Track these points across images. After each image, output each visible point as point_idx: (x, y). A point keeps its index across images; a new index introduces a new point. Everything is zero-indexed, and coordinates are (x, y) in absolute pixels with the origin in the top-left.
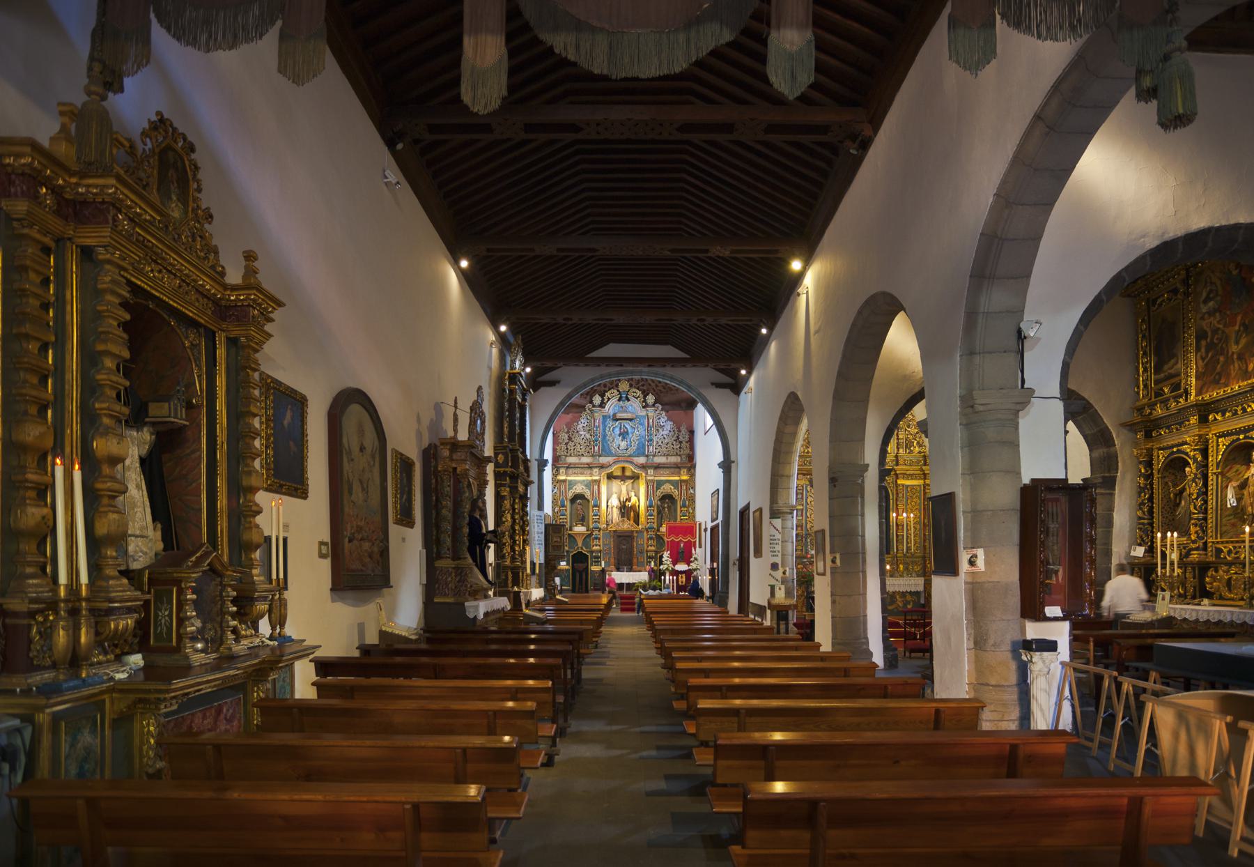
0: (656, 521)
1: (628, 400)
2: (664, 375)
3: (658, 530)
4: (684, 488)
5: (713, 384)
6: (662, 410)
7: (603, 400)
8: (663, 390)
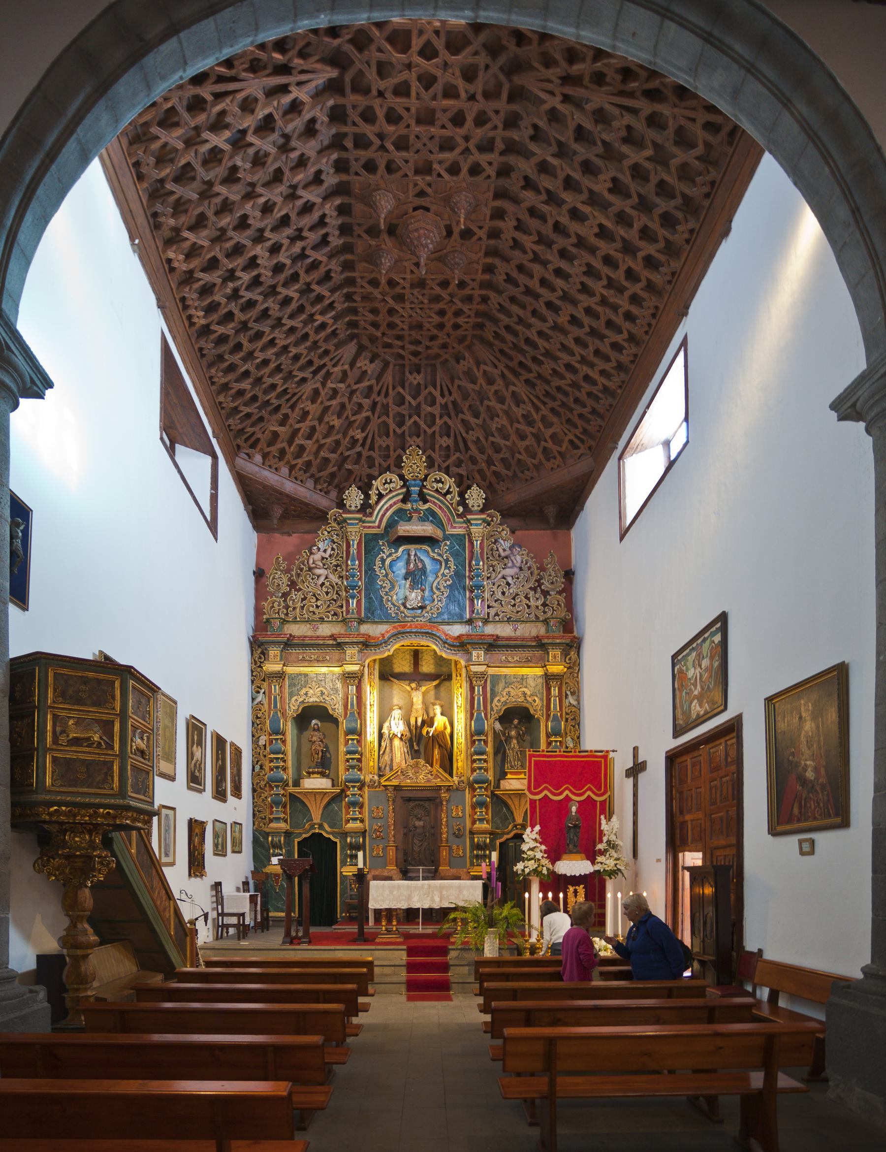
3: (498, 786)
7: (367, 496)
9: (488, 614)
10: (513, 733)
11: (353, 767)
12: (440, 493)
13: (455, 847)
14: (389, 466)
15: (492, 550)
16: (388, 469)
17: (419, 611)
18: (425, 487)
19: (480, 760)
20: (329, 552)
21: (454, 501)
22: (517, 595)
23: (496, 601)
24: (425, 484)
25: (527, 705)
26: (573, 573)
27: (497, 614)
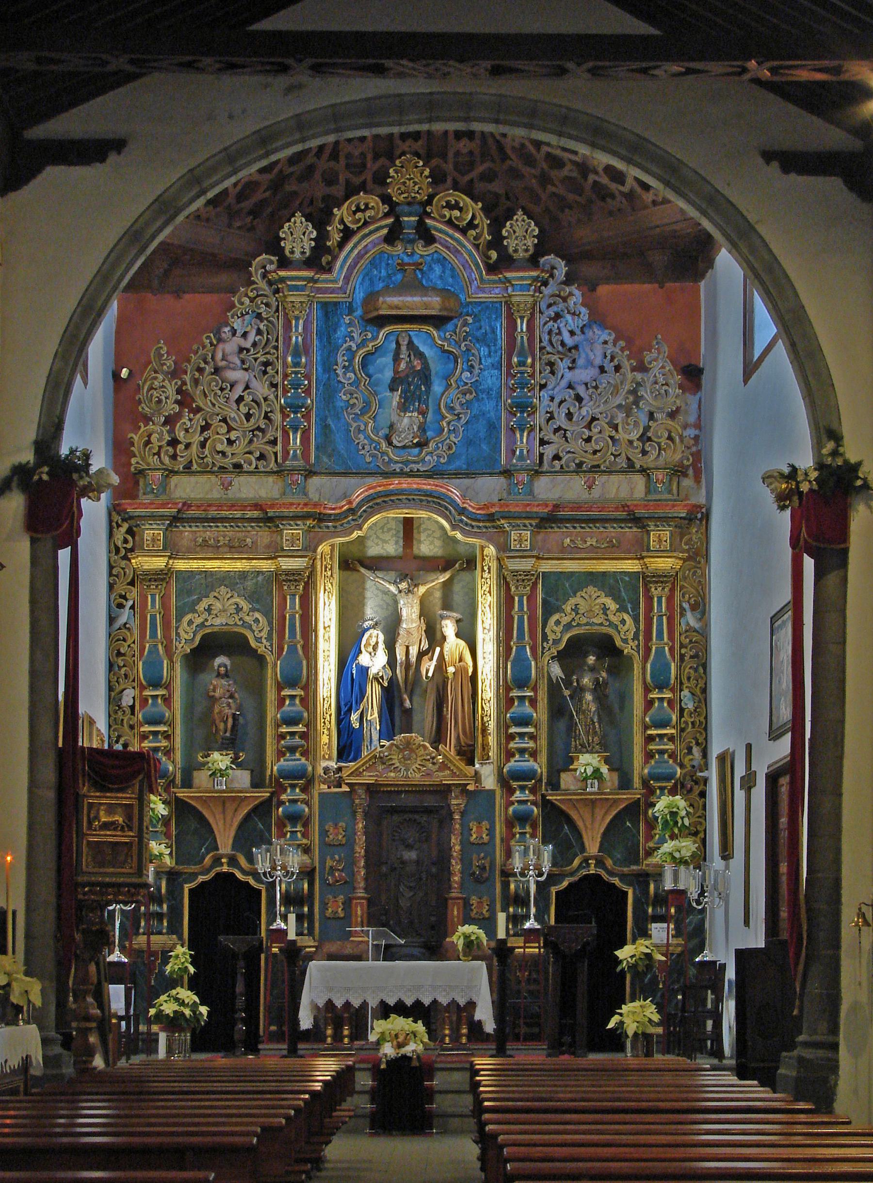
0: (543, 742)
1: (429, 239)
2: (564, 120)
3: (554, 785)
4: (660, 607)
5: (768, 156)
6: (569, 280)
7: (322, 236)
8: (571, 197)
9: (541, 455)
10: (586, 681)
11: (292, 750)
12: (456, 228)
13: (474, 900)
14: (364, 183)
15: (550, 332)
16: (363, 187)
17: (416, 451)
18: (428, 215)
19: (522, 735)
20: (252, 337)
21: (482, 240)
22: (594, 419)
23: (556, 430)
24: (428, 209)
25: (611, 631)
26: (700, 371)
27: (557, 457)
